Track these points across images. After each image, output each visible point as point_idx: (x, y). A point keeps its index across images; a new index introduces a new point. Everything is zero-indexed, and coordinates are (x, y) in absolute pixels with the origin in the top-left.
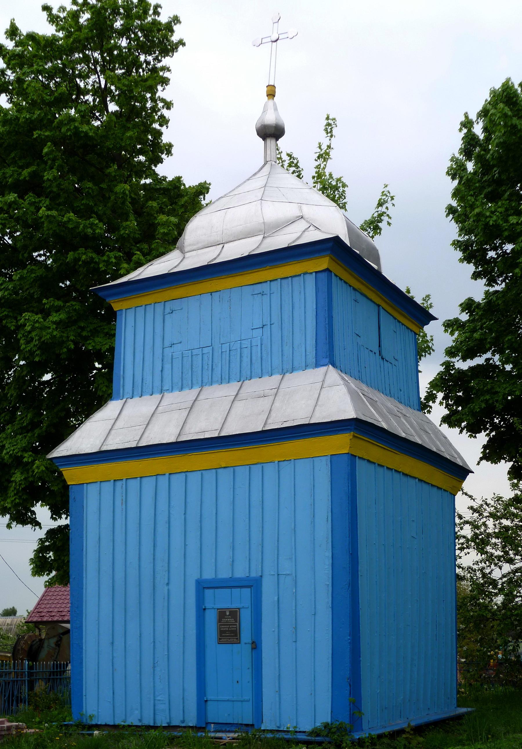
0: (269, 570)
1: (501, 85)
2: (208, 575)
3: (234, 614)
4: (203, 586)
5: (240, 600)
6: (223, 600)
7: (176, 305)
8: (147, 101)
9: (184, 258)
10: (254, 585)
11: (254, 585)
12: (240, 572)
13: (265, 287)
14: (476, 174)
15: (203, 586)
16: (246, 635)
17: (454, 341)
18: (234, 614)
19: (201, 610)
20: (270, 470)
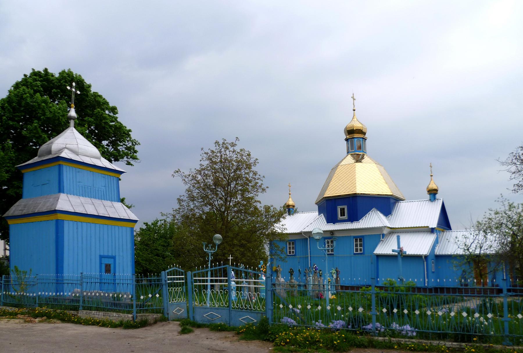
0: (117, 254)
1: (108, 101)
2: (102, 254)
3: (110, 265)
4: (101, 257)
5: (110, 261)
6: (106, 261)
7: (80, 170)
8: (325, 325)
9: (65, 148)
10: (114, 258)
11: (114, 258)
12: (110, 254)
13: (107, 176)
14: (327, 333)
15: (101, 257)
16: (112, 271)
17: (325, 299)
18: (110, 265)
19: (101, 264)
20: (117, 228)
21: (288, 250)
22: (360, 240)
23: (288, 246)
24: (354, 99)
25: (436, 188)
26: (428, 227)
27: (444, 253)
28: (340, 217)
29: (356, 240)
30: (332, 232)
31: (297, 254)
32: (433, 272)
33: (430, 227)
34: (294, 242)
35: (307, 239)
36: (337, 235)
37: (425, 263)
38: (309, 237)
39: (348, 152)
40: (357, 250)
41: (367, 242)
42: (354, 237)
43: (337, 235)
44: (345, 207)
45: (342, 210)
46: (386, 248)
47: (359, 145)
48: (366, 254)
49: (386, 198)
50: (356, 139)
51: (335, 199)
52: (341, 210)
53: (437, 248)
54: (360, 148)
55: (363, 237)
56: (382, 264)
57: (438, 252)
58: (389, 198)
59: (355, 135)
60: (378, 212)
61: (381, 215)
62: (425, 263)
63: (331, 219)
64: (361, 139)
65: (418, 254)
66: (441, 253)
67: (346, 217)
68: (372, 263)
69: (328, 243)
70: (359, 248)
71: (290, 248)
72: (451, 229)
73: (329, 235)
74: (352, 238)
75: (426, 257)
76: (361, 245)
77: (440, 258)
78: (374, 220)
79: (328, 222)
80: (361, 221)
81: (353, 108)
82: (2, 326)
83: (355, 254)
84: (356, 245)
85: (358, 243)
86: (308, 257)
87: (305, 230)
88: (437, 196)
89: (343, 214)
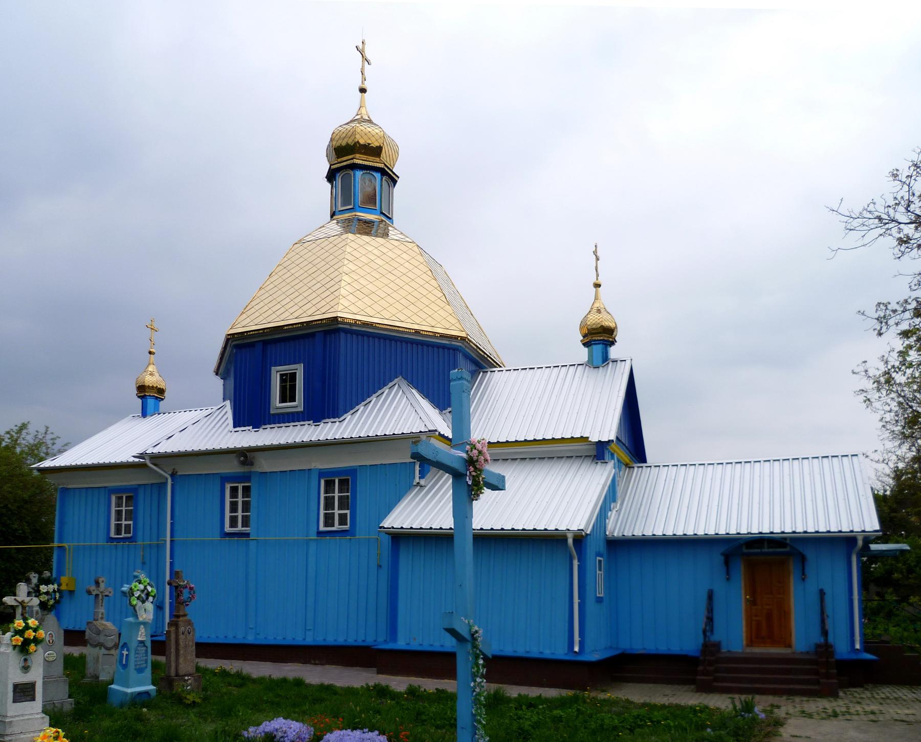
21: (113, 522)
22: (344, 484)
23: (113, 509)
24: (365, 60)
25: (612, 325)
26: (584, 439)
27: (638, 533)
28: (276, 404)
29: (329, 485)
30: (245, 455)
31: (140, 534)
32: (599, 600)
33: (594, 438)
34: (131, 495)
35: (162, 486)
36: (264, 465)
37: (576, 563)
38: (173, 475)
39: (333, 215)
40: (329, 520)
41: (364, 489)
42: (322, 474)
43: (264, 465)
44: (299, 370)
45: (288, 381)
46: (427, 509)
47: (369, 190)
48: (361, 534)
49: (444, 347)
50: (359, 174)
51: (265, 343)
52: (283, 381)
53: (612, 515)
54: (371, 199)
55: (352, 471)
56: (414, 569)
57: (617, 527)
58: (455, 349)
59: (358, 156)
60: (414, 391)
61: (425, 404)
62: (576, 563)
63: (250, 410)
64: (378, 175)
65: (552, 527)
66: (628, 533)
67: (298, 404)
68: (380, 566)
69: (234, 491)
70: (337, 512)
71: (119, 513)
72: (645, 461)
73: (232, 467)
74: (315, 477)
75: (580, 539)
76: (343, 504)
77: (623, 548)
78: (398, 412)
79: (238, 422)
80: (348, 416)
81: (359, 84)
82: (2, 650)
83: (320, 533)
84: (329, 504)
85: (337, 495)
86: (160, 547)
87: (156, 450)
88: (614, 352)
89: (288, 394)
